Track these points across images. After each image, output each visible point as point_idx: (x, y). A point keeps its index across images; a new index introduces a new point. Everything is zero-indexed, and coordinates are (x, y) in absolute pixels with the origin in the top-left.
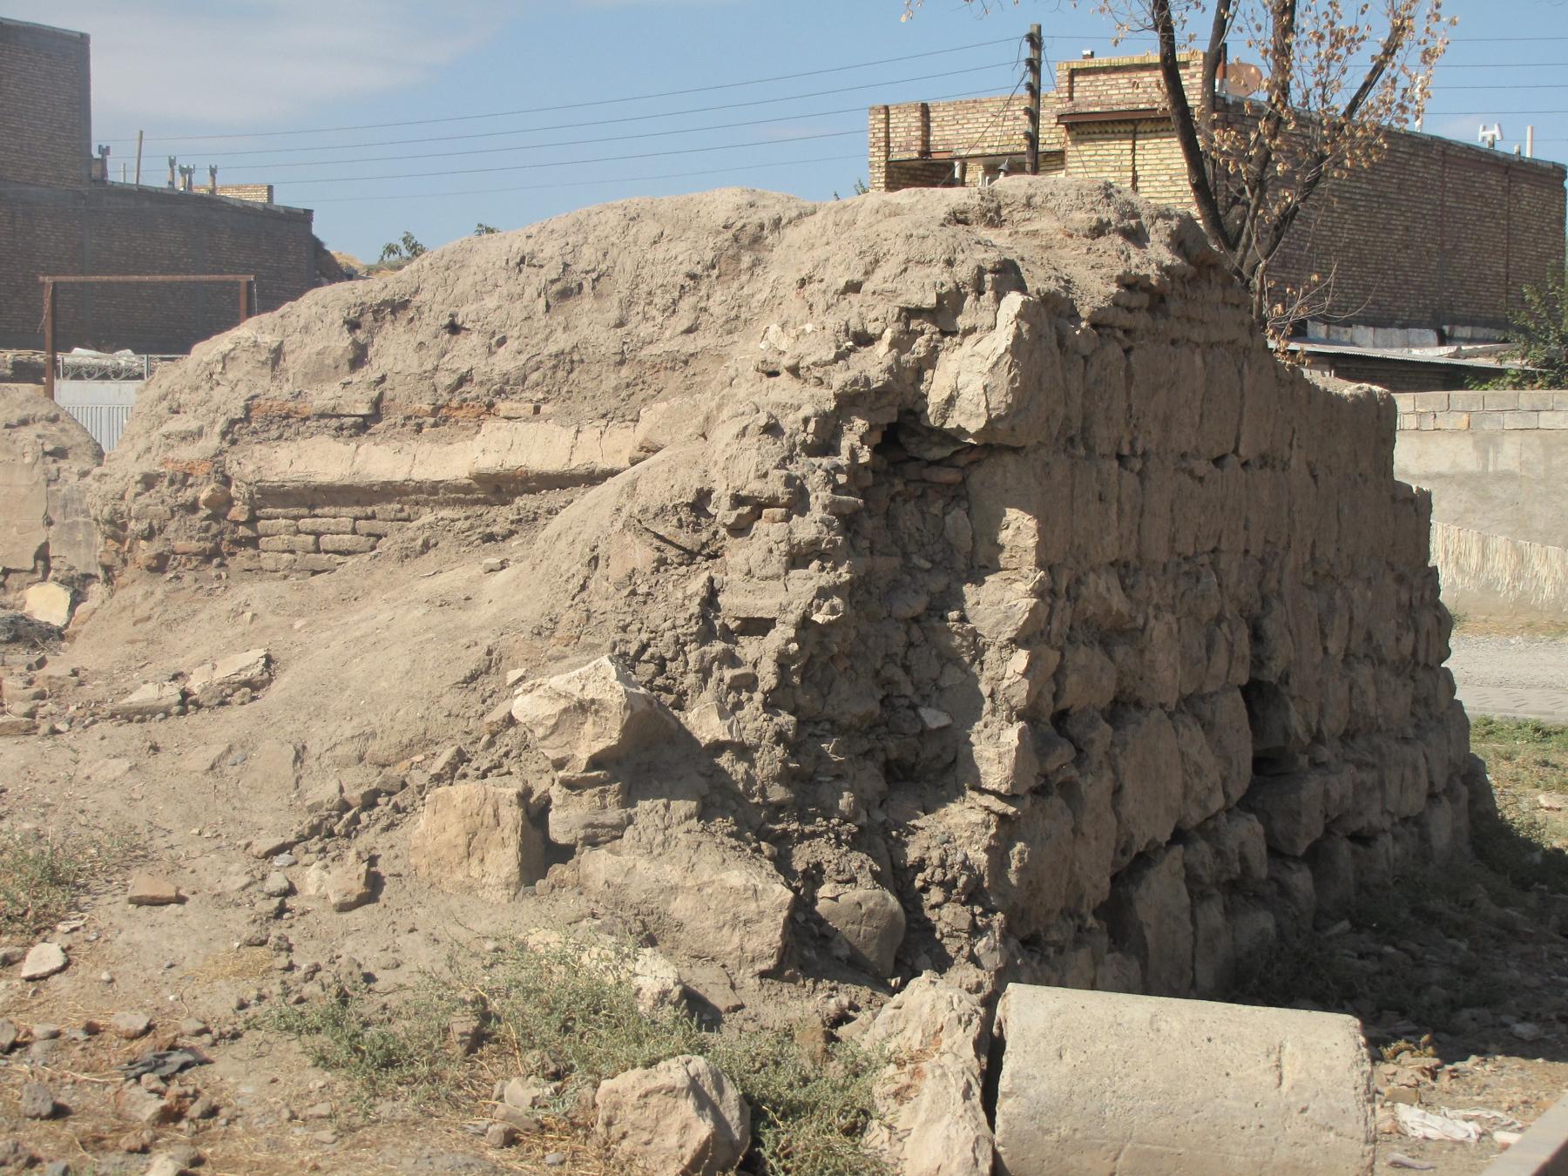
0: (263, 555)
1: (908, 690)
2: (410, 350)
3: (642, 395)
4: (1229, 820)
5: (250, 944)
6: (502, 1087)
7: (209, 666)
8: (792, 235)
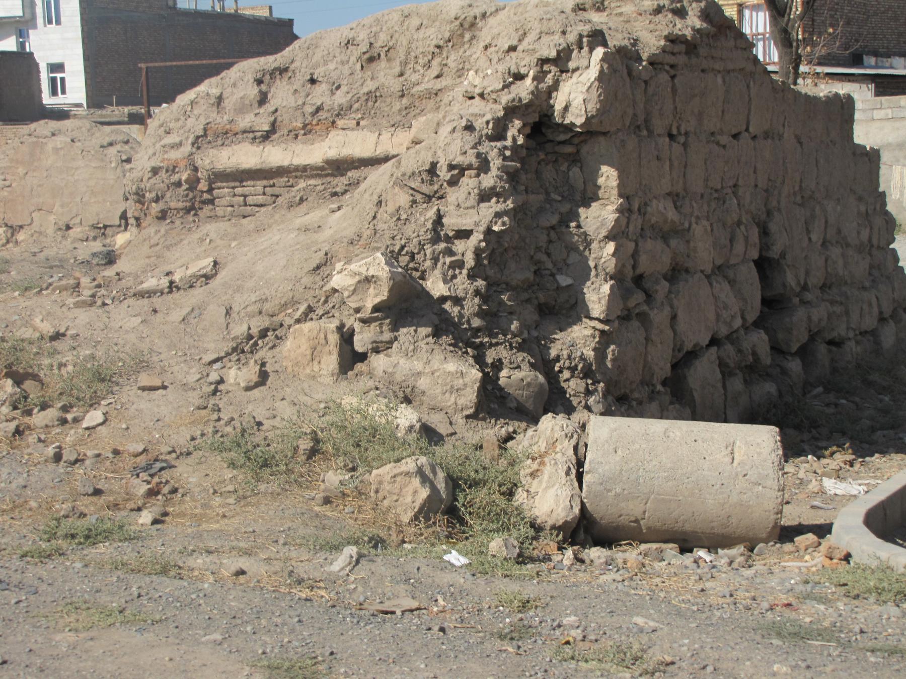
0: (217, 209)
1: (550, 266)
2: (290, 94)
3: (413, 114)
4: (746, 334)
5: (199, 408)
6: (324, 476)
7: (184, 268)
8: (492, 21)
